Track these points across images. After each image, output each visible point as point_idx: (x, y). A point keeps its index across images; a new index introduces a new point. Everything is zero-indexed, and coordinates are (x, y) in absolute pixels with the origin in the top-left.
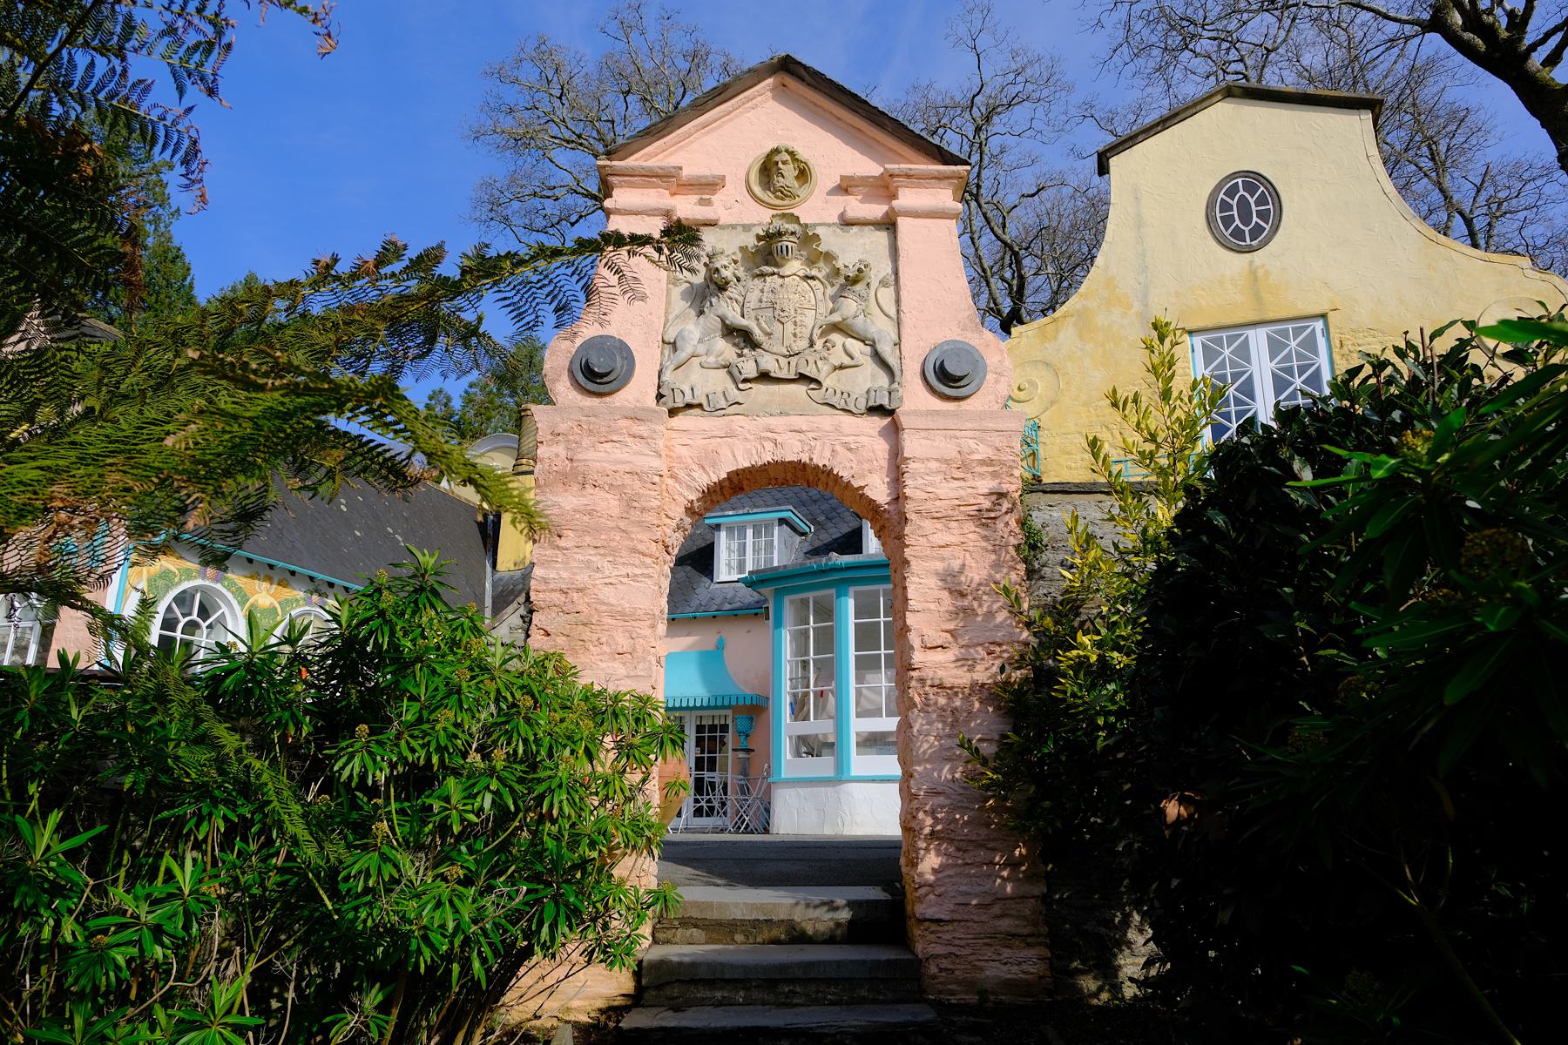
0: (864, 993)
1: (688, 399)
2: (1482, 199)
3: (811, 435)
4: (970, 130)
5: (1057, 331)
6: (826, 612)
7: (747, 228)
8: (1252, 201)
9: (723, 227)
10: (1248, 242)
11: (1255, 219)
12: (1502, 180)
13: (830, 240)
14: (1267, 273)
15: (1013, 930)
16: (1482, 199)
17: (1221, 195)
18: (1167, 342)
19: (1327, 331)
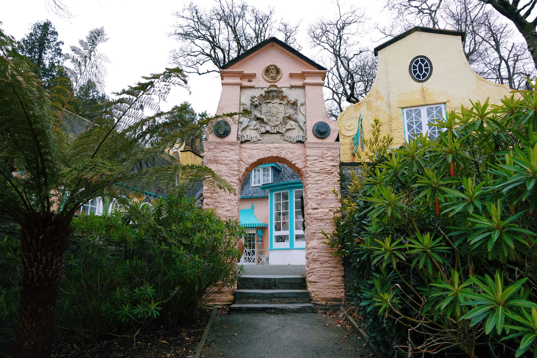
0: (294, 300)
1: (246, 139)
2: (511, 55)
3: (280, 149)
4: (336, 32)
5: (360, 107)
6: (286, 197)
7: (262, 88)
8: (423, 65)
9: (255, 88)
10: (422, 79)
11: (424, 71)
12: (518, 49)
13: (286, 92)
14: (427, 89)
15: (336, 285)
16: (511, 55)
17: (413, 64)
18: (378, 125)
19: (445, 108)
